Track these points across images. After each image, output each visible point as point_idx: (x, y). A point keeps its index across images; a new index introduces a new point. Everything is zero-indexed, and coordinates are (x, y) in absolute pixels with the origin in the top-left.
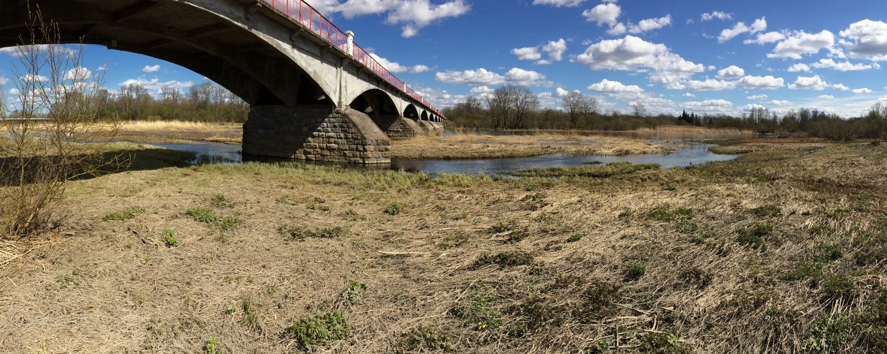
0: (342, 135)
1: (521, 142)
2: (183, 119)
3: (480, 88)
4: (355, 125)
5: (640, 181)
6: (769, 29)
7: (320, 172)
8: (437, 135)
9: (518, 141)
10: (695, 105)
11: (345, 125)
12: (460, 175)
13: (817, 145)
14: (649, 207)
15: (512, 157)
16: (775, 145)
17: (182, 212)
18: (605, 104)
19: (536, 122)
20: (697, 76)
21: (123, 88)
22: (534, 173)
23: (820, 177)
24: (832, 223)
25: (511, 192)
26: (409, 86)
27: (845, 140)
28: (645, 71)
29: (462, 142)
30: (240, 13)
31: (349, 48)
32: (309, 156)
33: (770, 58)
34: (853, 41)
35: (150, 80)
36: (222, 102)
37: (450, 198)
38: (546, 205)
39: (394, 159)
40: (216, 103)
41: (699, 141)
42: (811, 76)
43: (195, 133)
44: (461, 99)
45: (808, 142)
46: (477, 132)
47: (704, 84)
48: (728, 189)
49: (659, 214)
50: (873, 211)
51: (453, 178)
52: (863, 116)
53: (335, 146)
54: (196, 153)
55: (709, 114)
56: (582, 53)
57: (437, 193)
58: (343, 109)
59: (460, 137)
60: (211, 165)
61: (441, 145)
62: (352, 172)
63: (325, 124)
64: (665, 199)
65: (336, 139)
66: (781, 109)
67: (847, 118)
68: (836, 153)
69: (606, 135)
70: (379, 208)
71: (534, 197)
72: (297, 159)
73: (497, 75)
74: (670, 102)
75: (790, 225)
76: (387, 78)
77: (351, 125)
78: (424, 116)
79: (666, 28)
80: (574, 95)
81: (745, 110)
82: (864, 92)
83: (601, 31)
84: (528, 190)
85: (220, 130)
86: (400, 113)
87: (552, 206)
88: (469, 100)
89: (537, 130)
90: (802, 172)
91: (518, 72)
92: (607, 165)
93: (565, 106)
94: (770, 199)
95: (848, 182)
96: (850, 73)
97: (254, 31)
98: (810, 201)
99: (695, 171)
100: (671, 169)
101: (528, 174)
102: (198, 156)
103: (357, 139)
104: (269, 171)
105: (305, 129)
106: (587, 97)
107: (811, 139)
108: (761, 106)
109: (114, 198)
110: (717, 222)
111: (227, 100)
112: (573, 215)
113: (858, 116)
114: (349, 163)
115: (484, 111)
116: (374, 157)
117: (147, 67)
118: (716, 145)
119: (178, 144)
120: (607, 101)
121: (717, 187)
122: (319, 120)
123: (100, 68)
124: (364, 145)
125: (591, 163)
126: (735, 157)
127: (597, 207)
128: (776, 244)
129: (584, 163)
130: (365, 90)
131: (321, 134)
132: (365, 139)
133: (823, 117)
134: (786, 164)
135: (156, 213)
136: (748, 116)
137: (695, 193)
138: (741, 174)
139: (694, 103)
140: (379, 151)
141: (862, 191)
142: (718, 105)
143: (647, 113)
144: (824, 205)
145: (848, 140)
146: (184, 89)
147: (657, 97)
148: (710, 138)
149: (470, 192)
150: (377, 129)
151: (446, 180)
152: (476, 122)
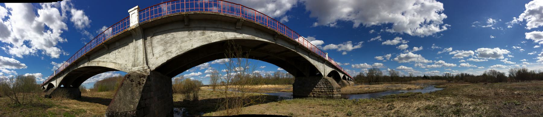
0: (326, 86)
2: (272, 84)
4: (330, 83)
6: (453, 50)
7: (320, 100)
10: (428, 73)
13: (468, 84)
16: (454, 85)
18: (402, 73)
21: (254, 74)
27: (476, 83)
29: (361, 87)
32: (314, 95)
36: (284, 77)
37: (365, 108)
40: (282, 78)
45: (464, 83)
47: (431, 66)
49: (427, 108)
52: (481, 75)
53: (323, 90)
55: (432, 75)
56: (396, 58)
58: (325, 77)
59: (360, 86)
60: (284, 100)
61: (355, 89)
63: (320, 83)
64: (428, 103)
68: (474, 87)
72: (310, 96)
73: (370, 65)
74: (421, 72)
75: (466, 109)
77: (328, 82)
80: (392, 70)
81: (444, 74)
82: (482, 68)
83: (403, 51)
85: (284, 87)
88: (360, 73)
90: (465, 93)
91: (377, 64)
95: (479, 95)
96: (478, 62)
97: (298, 53)
103: (330, 87)
105: (313, 85)
108: (449, 72)
113: (479, 75)
116: (336, 94)
119: (272, 93)
121: (441, 98)
127: (409, 107)
128: (463, 115)
130: (331, 71)
131: (318, 86)
133: (469, 75)
136: (444, 76)
139: (428, 72)
142: (435, 72)
143: (413, 76)
145: (477, 83)
146: (272, 73)
147: (417, 71)
149: (371, 105)
150: (336, 84)
152: (363, 81)
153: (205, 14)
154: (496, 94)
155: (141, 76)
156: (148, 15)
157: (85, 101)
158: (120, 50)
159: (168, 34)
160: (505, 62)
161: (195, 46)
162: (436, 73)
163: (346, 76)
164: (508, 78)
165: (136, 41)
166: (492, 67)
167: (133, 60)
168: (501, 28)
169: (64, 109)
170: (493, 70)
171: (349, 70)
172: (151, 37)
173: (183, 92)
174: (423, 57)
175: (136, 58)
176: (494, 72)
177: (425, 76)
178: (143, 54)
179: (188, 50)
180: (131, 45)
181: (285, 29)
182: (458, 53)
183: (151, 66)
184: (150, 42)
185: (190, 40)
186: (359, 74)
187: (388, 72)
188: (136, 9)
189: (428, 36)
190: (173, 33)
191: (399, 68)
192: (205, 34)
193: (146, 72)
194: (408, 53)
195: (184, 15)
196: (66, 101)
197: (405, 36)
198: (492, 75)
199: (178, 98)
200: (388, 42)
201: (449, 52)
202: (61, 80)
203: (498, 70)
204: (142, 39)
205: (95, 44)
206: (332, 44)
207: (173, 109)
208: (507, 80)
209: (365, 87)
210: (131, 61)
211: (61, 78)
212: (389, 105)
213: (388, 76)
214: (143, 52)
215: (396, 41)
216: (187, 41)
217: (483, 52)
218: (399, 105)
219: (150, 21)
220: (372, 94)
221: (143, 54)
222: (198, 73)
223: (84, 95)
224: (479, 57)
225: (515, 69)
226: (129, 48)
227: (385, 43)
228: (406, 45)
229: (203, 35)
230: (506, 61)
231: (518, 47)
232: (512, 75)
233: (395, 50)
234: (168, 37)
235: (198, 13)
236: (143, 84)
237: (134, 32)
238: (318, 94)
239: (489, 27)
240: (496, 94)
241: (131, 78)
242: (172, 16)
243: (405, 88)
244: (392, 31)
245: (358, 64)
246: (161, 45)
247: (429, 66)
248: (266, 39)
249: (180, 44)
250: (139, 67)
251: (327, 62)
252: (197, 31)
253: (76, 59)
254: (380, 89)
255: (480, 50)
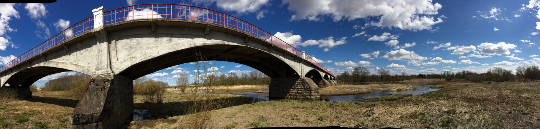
1: (364, 87)
3: (350, 68)
4: (307, 83)
5: (406, 101)
6: (451, 46)
7: (296, 103)
8: (335, 85)
9: (363, 87)
10: (424, 71)
11: (303, 83)
12: (344, 102)
13: (469, 84)
14: (409, 113)
15: (361, 94)
16: (453, 84)
17: (249, 124)
19: (369, 80)
20: (425, 61)
22: (369, 100)
23: (470, 97)
24: (475, 116)
25: (361, 109)
26: (326, 68)
28: (406, 60)
30: (267, 49)
31: (304, 56)
33: (452, 55)
34: (482, 49)
35: (238, 70)
36: (261, 77)
37: (341, 113)
38: (374, 114)
39: (321, 96)
41: (426, 84)
42: (467, 60)
43: (252, 89)
44: (343, 72)
46: (349, 84)
47: (427, 64)
48: (437, 103)
50: (490, 110)
51: (341, 103)
52: (485, 73)
53: (300, 91)
54: (253, 97)
55: (429, 74)
57: (336, 110)
59: (343, 86)
60: (259, 102)
61: (337, 90)
62: (307, 102)
64: (415, 109)
65: (301, 89)
66: (455, 71)
67: (479, 73)
69: (393, 83)
70: (317, 117)
71: (369, 111)
72: (287, 98)
73: (356, 63)
74: (415, 70)
75: (460, 118)
76: (318, 66)
77: (306, 83)
78: (331, 78)
79: (414, 47)
80: (382, 69)
81: (442, 72)
82: (486, 65)
83: (392, 48)
84: (367, 108)
86: (322, 77)
87: (376, 114)
88: (345, 72)
89: (369, 82)
90: (464, 95)
91: (363, 62)
92: (394, 95)
93: (378, 73)
94: (452, 106)
95: (480, 98)
96: (481, 58)
97: (271, 54)
98: (467, 107)
99: (425, 96)
100: (416, 96)
101: (367, 100)
102: (254, 99)
104: (278, 103)
106: (386, 70)
107: (466, 81)
108: (448, 70)
109: (228, 119)
110: (434, 118)
111: (263, 76)
112: (383, 118)
113: (483, 73)
114: (306, 98)
115: (351, 76)
116: (315, 96)
117: (237, 66)
118: (432, 85)
119: (248, 94)
120: (394, 71)
121: (433, 102)
122: (294, 82)
123: (222, 67)
124: (310, 91)
125: (388, 95)
126: (439, 89)
129: (386, 95)
130: (310, 70)
131: (295, 87)
132: (311, 88)
133: (471, 73)
134: (457, 92)
135: (241, 125)
136: (443, 74)
137: (425, 105)
138: (442, 96)
139: (424, 70)
140: (316, 92)
141: (486, 102)
142: (432, 70)
143: (407, 75)
144: (472, 108)
145: (480, 81)
146: (248, 73)
148: (430, 82)
149: (347, 109)
150: (315, 84)
151: (339, 104)
153: (172, 21)
154: (500, 97)
155: (105, 81)
156: (113, 18)
157: (37, 102)
158: (82, 51)
159: (133, 39)
160: (512, 58)
161: (161, 53)
162: (433, 71)
163: (328, 76)
164: (516, 77)
165: (100, 44)
166: (497, 63)
167: (97, 63)
168: (506, 19)
169: (12, 112)
170: (498, 67)
171: (333, 68)
172: (116, 41)
173: (145, 93)
174: (416, 54)
175: (99, 61)
176: (500, 70)
177: (420, 74)
178: (107, 57)
179: (154, 56)
180: (94, 47)
181: (256, 30)
182: (458, 48)
183: (114, 70)
184: (114, 46)
185: (157, 47)
186: (344, 73)
187: (377, 71)
188: (101, 9)
189: (421, 30)
190: (138, 38)
191: (390, 66)
192: (172, 40)
193: (109, 76)
194: (399, 49)
195: (152, 22)
196: (13, 102)
197: (394, 31)
198: (497, 72)
199: (138, 99)
200: (375, 38)
201: (447, 48)
202: (8, 79)
203: (504, 68)
204: (106, 42)
205: (54, 43)
206: (311, 40)
207: (133, 111)
208: (514, 79)
209: (347, 88)
210: (94, 65)
211: (7, 76)
212: (367, 111)
213: (377, 75)
214: (107, 56)
215: (384, 37)
216: (153, 47)
217: (487, 48)
218: (379, 111)
219: (116, 24)
220: (358, 96)
221: (107, 58)
222: (162, 73)
223: (34, 94)
224: (482, 53)
225: (524, 67)
226: (93, 51)
227: (372, 39)
228: (396, 40)
229: (170, 42)
230: (512, 57)
231: (527, 41)
232: (519, 73)
233: (384, 47)
234: (133, 42)
235: (166, 20)
236: (107, 88)
237: (98, 35)
238: (295, 95)
239: (492, 18)
240: (500, 97)
241: (96, 83)
242: (138, 22)
243: (395, 88)
244: (379, 24)
245: (342, 61)
246: (126, 50)
247: (424, 63)
248: (236, 43)
249: (145, 50)
250: (103, 71)
251: (304, 61)
252: (164, 38)
253: (30, 57)
254: (364, 90)
255: (483, 46)
